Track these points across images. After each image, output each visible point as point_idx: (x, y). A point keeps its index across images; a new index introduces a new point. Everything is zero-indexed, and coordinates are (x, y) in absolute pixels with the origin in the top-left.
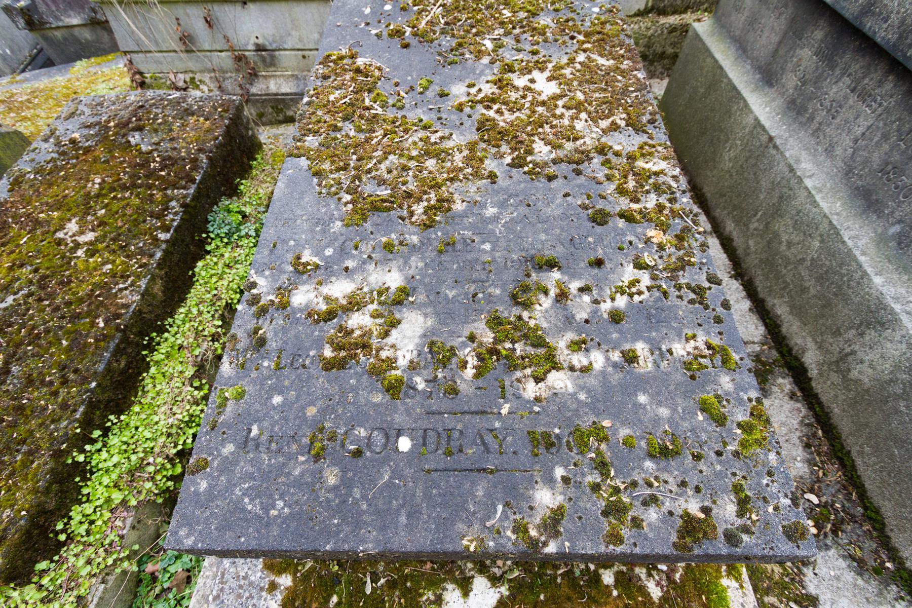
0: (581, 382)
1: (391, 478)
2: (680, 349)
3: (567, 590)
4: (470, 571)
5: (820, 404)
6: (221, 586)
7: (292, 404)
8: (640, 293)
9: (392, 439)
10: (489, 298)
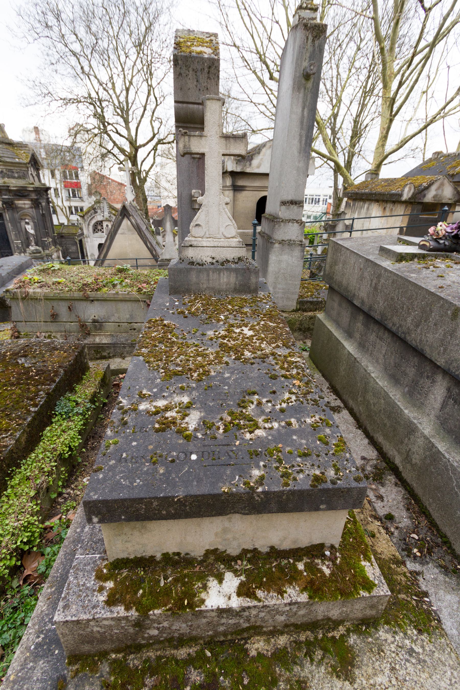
0: (269, 433)
1: (188, 469)
2: (309, 421)
3: (278, 574)
4: (222, 569)
5: (408, 484)
6: (67, 591)
7: (141, 445)
8: (291, 402)
9: (189, 455)
10: (228, 405)
